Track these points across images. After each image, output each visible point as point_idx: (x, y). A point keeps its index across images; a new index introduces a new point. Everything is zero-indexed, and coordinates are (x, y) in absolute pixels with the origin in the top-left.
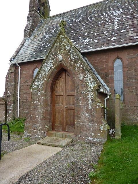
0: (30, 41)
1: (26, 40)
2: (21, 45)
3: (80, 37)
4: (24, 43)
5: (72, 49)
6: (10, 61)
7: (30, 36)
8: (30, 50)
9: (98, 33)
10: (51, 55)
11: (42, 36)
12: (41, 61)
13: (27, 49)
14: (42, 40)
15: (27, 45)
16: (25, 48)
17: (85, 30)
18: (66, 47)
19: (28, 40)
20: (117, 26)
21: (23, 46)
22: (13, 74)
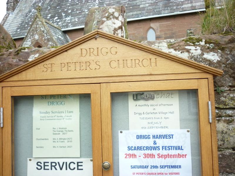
0: (14, 16)
2: (3, 19)
3: (64, 14)
4: (7, 17)
5: (45, 30)
8: (14, 26)
9: (80, 11)
10: (29, 35)
11: (27, 11)
12: (22, 39)
13: (11, 25)
14: (26, 15)
15: (11, 21)
16: (8, 23)
17: (70, 7)
18: (41, 29)
19: (12, 14)
20: (97, 5)
21: (6, 21)
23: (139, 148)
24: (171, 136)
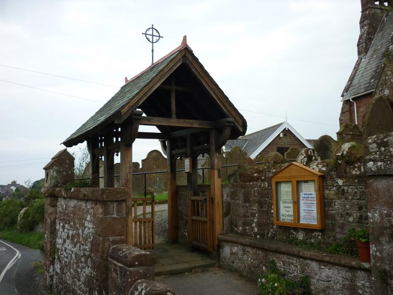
1: (361, 59)
2: (355, 68)
6: (342, 96)
7: (366, 52)
13: (364, 74)
16: (361, 72)
21: (357, 70)
22: (348, 113)
23: (305, 198)
24: (311, 194)
